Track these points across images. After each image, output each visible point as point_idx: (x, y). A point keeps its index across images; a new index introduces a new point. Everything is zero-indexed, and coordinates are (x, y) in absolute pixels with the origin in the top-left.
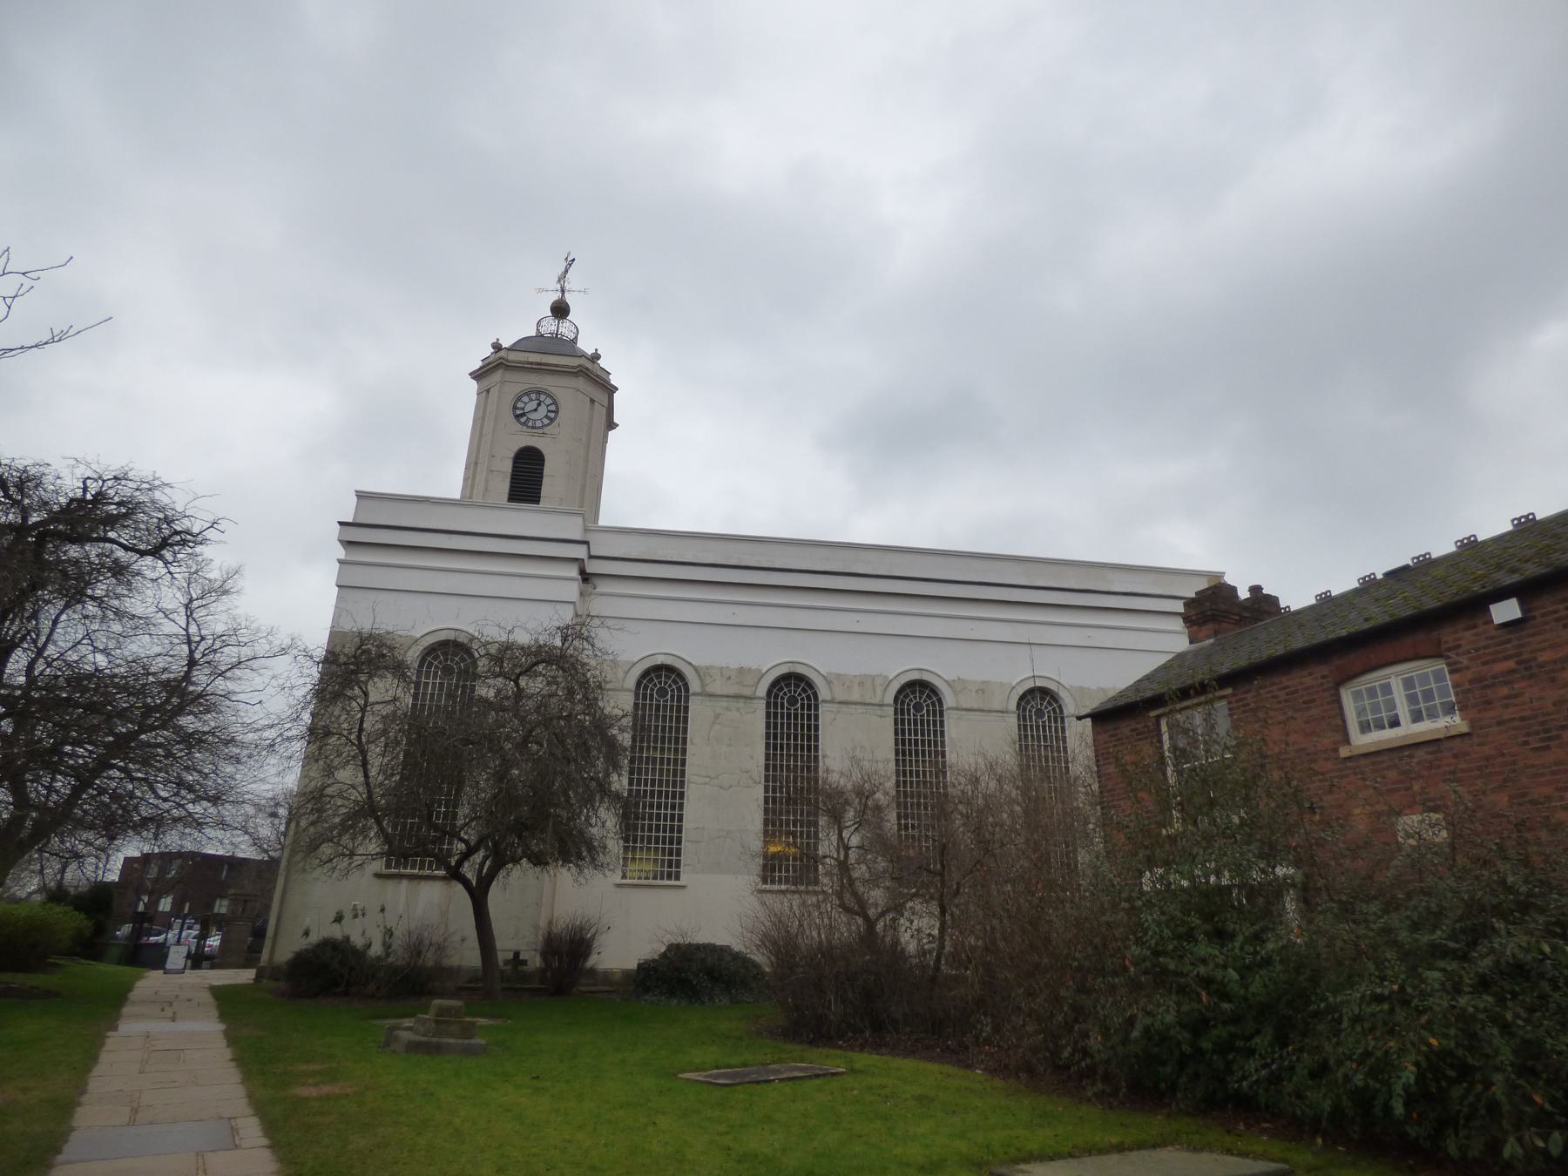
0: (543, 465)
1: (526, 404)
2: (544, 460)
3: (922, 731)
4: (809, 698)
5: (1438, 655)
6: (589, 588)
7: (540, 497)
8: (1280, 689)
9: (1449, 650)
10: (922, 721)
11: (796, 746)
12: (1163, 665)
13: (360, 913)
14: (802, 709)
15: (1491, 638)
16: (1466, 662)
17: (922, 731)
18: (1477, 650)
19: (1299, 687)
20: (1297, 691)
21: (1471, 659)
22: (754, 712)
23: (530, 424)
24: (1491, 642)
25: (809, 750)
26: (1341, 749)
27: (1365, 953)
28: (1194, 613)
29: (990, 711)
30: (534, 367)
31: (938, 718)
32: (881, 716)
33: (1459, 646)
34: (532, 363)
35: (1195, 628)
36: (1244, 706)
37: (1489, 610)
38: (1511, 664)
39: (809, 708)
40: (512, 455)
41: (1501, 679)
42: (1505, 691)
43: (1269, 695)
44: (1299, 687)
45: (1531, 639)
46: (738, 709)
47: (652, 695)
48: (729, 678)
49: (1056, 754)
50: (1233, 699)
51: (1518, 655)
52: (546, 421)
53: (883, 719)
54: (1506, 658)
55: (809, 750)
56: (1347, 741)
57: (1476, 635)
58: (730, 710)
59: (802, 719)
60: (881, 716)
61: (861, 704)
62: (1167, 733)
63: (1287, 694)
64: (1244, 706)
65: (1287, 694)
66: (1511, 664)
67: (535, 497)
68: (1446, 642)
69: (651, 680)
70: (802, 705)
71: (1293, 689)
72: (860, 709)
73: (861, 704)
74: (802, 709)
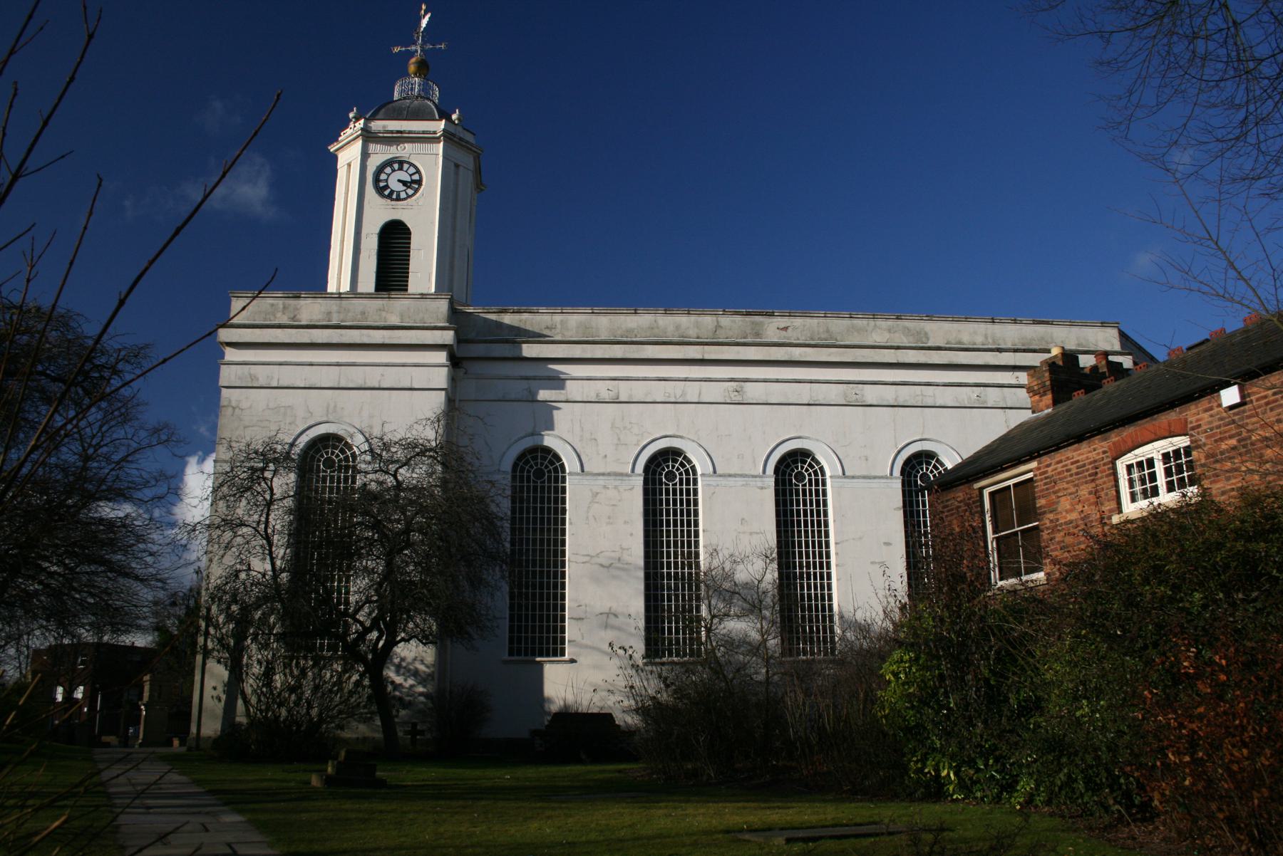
0: (410, 239)
1: (389, 175)
2: (410, 233)
3: (805, 502)
4: (687, 472)
5: (1185, 435)
6: (461, 372)
7: (408, 273)
8: (1072, 464)
9: (1193, 429)
10: (804, 491)
11: (675, 521)
12: (1005, 435)
13: (611, 521)
14: (681, 484)
15: (1221, 419)
16: (1203, 440)
17: (805, 502)
18: (1211, 430)
19: (1086, 462)
20: (1084, 465)
21: (1207, 437)
22: (633, 488)
23: (394, 196)
24: (1222, 422)
25: (689, 525)
26: (1113, 518)
27: (227, 613)
28: (1036, 383)
29: (875, 477)
30: (395, 135)
31: (820, 487)
32: (762, 488)
33: (1199, 426)
34: (392, 132)
35: (1037, 397)
36: (1046, 478)
37: (1219, 395)
38: (1233, 442)
39: (688, 483)
40: (377, 230)
41: (1227, 455)
42: (1229, 465)
43: (1064, 469)
44: (1086, 462)
45: (1248, 421)
46: (616, 487)
47: (529, 477)
48: (606, 456)
49: (524, 602)
50: (1038, 473)
51: (1239, 434)
52: (406, 166)
53: (764, 490)
54: (1231, 437)
55: (689, 525)
56: (1120, 511)
57: (1211, 416)
58: (608, 488)
59: (681, 494)
60: (762, 488)
61: (741, 476)
62: (148, 683)
63: (1078, 468)
64: (1046, 478)
65: (1078, 468)
66: (1233, 442)
67: (405, 234)
68: (1191, 422)
69: (527, 462)
70: (681, 480)
71: (1081, 463)
72: (740, 481)
73: (741, 476)
74: (681, 484)
